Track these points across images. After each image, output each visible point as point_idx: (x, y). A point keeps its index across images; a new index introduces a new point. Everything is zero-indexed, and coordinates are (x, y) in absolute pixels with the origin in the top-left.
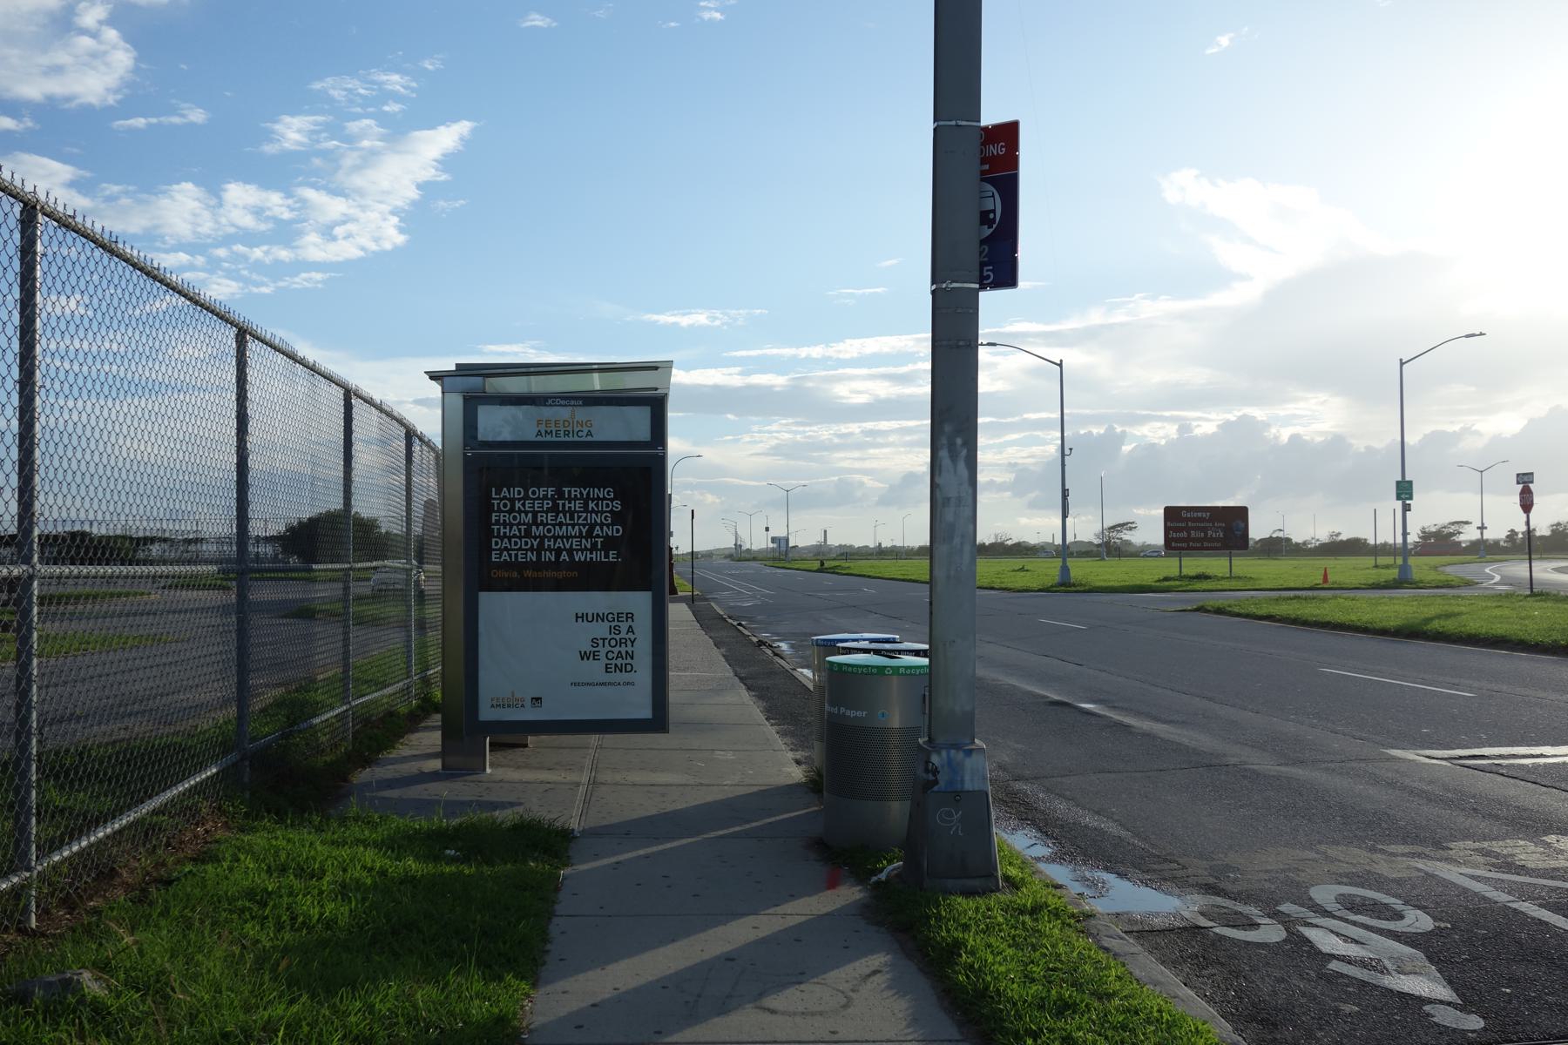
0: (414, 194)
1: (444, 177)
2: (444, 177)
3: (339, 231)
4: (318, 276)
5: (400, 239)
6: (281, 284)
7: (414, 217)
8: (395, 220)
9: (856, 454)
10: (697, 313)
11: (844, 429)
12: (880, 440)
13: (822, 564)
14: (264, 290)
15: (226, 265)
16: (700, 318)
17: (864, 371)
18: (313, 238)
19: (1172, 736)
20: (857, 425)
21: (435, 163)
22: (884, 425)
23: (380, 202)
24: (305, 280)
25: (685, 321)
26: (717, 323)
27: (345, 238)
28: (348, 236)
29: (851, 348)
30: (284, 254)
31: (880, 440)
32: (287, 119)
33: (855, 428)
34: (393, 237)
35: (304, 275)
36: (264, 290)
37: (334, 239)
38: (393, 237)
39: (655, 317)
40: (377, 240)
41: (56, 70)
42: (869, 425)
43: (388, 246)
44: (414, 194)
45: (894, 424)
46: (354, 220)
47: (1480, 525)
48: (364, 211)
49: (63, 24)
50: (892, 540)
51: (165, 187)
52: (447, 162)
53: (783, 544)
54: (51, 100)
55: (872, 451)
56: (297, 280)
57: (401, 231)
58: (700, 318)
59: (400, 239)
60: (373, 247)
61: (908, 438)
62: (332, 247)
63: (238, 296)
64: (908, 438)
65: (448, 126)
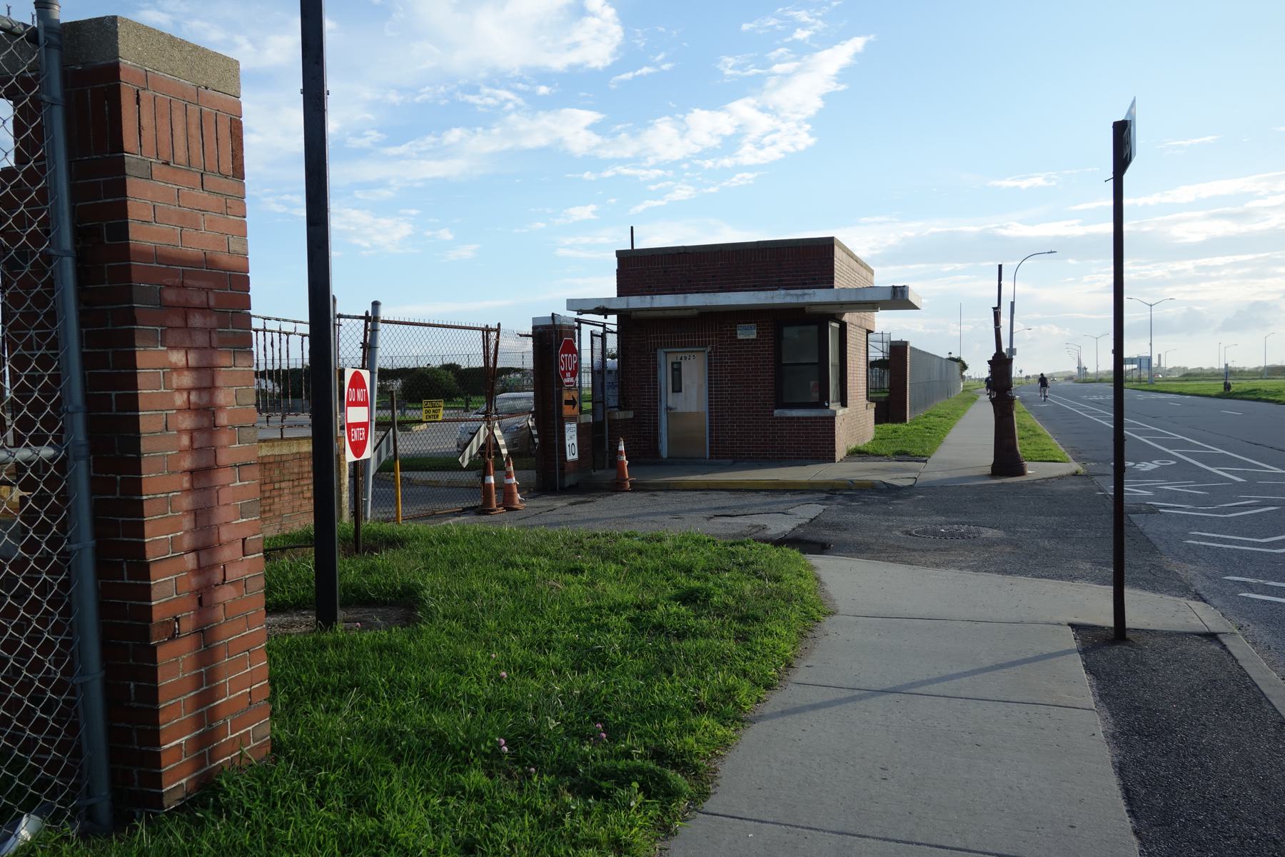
0: (819, 104)
1: (842, 87)
2: (842, 87)
3: (767, 140)
4: (747, 175)
5: (811, 141)
6: (725, 184)
7: (818, 123)
8: (808, 127)
9: (1188, 288)
10: (1034, 177)
11: (1178, 266)
12: (1213, 274)
13: (1227, 387)
14: (712, 190)
15: (688, 174)
16: (1039, 181)
17: (1200, 214)
18: (748, 147)
19: (781, 499)
20: (1191, 262)
21: (835, 78)
22: (1219, 261)
23: (796, 113)
24: (740, 180)
25: (1025, 184)
26: (1054, 183)
27: (770, 145)
28: (773, 143)
29: (1185, 193)
30: (727, 162)
31: (1213, 274)
32: (726, 59)
33: (1189, 265)
34: (805, 140)
35: (739, 176)
36: (712, 190)
37: (762, 147)
38: (805, 140)
39: (999, 183)
40: (793, 145)
41: (575, 45)
42: (1202, 262)
43: (801, 147)
44: (819, 104)
45: (1230, 259)
46: (777, 131)
47: (384, 314)
48: (784, 122)
49: (579, 11)
50: (950, 353)
51: (651, 121)
52: (844, 75)
53: (1144, 364)
54: (573, 68)
55: (1203, 285)
56: (734, 180)
57: (811, 134)
58: (1039, 181)
59: (811, 141)
60: (792, 150)
61: (1240, 271)
62: (762, 153)
63: (693, 197)
64: (1240, 271)
65: (843, 44)
